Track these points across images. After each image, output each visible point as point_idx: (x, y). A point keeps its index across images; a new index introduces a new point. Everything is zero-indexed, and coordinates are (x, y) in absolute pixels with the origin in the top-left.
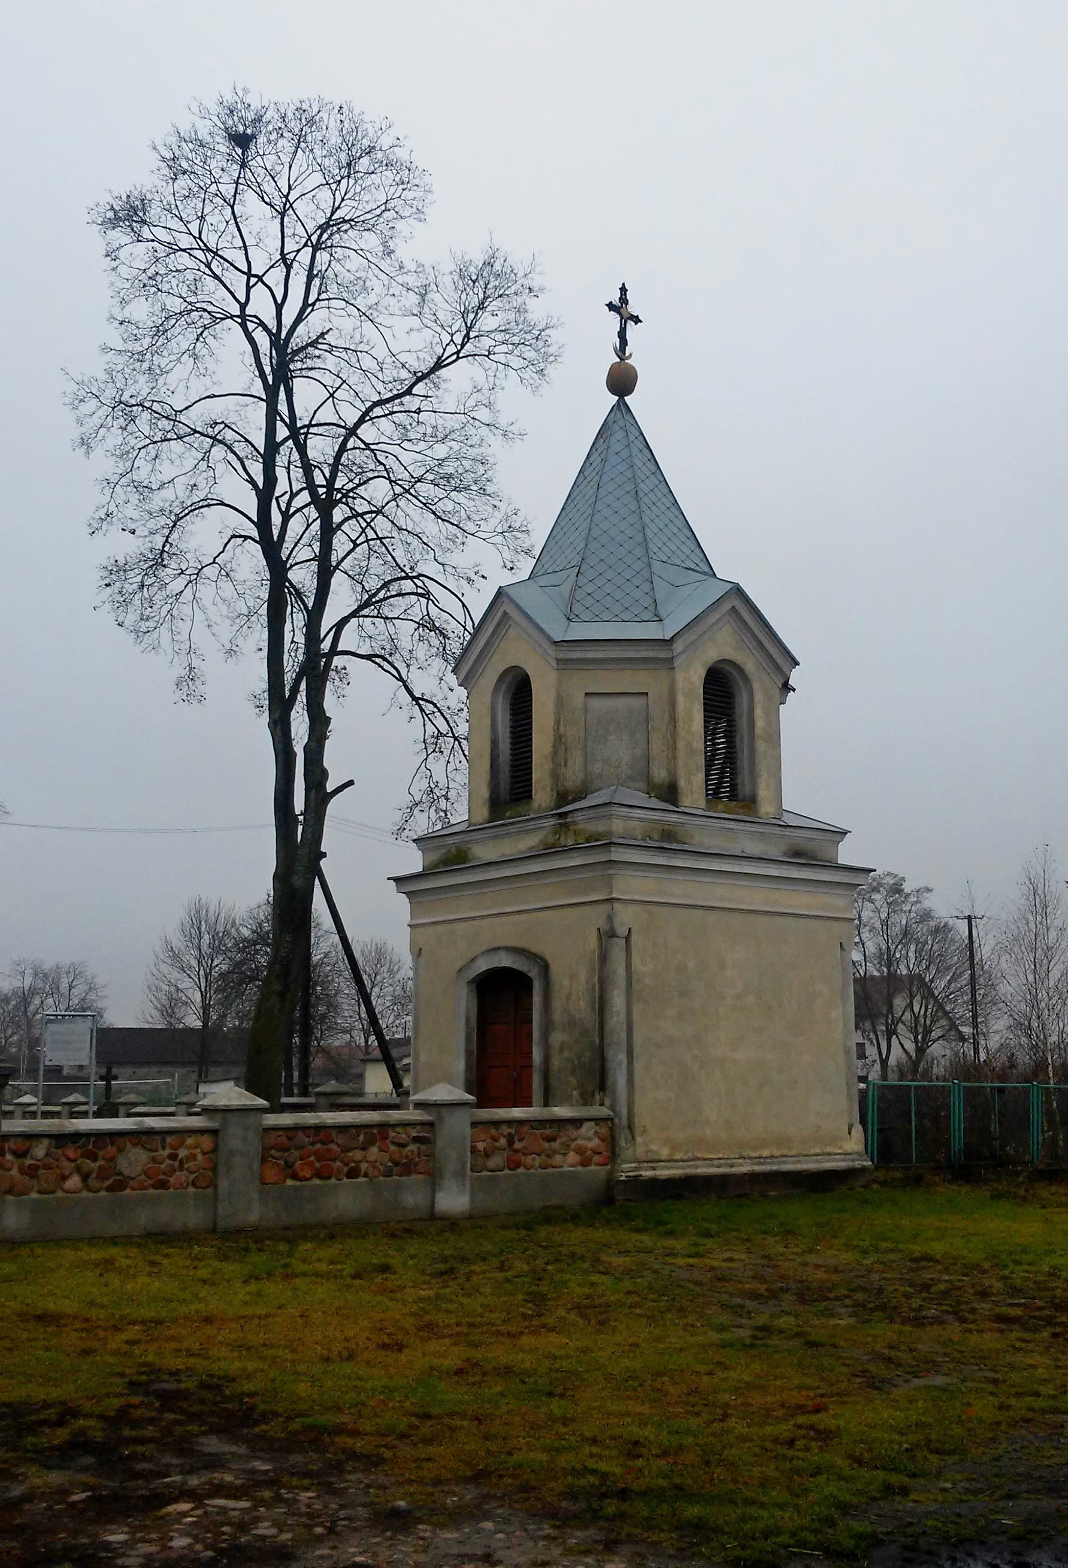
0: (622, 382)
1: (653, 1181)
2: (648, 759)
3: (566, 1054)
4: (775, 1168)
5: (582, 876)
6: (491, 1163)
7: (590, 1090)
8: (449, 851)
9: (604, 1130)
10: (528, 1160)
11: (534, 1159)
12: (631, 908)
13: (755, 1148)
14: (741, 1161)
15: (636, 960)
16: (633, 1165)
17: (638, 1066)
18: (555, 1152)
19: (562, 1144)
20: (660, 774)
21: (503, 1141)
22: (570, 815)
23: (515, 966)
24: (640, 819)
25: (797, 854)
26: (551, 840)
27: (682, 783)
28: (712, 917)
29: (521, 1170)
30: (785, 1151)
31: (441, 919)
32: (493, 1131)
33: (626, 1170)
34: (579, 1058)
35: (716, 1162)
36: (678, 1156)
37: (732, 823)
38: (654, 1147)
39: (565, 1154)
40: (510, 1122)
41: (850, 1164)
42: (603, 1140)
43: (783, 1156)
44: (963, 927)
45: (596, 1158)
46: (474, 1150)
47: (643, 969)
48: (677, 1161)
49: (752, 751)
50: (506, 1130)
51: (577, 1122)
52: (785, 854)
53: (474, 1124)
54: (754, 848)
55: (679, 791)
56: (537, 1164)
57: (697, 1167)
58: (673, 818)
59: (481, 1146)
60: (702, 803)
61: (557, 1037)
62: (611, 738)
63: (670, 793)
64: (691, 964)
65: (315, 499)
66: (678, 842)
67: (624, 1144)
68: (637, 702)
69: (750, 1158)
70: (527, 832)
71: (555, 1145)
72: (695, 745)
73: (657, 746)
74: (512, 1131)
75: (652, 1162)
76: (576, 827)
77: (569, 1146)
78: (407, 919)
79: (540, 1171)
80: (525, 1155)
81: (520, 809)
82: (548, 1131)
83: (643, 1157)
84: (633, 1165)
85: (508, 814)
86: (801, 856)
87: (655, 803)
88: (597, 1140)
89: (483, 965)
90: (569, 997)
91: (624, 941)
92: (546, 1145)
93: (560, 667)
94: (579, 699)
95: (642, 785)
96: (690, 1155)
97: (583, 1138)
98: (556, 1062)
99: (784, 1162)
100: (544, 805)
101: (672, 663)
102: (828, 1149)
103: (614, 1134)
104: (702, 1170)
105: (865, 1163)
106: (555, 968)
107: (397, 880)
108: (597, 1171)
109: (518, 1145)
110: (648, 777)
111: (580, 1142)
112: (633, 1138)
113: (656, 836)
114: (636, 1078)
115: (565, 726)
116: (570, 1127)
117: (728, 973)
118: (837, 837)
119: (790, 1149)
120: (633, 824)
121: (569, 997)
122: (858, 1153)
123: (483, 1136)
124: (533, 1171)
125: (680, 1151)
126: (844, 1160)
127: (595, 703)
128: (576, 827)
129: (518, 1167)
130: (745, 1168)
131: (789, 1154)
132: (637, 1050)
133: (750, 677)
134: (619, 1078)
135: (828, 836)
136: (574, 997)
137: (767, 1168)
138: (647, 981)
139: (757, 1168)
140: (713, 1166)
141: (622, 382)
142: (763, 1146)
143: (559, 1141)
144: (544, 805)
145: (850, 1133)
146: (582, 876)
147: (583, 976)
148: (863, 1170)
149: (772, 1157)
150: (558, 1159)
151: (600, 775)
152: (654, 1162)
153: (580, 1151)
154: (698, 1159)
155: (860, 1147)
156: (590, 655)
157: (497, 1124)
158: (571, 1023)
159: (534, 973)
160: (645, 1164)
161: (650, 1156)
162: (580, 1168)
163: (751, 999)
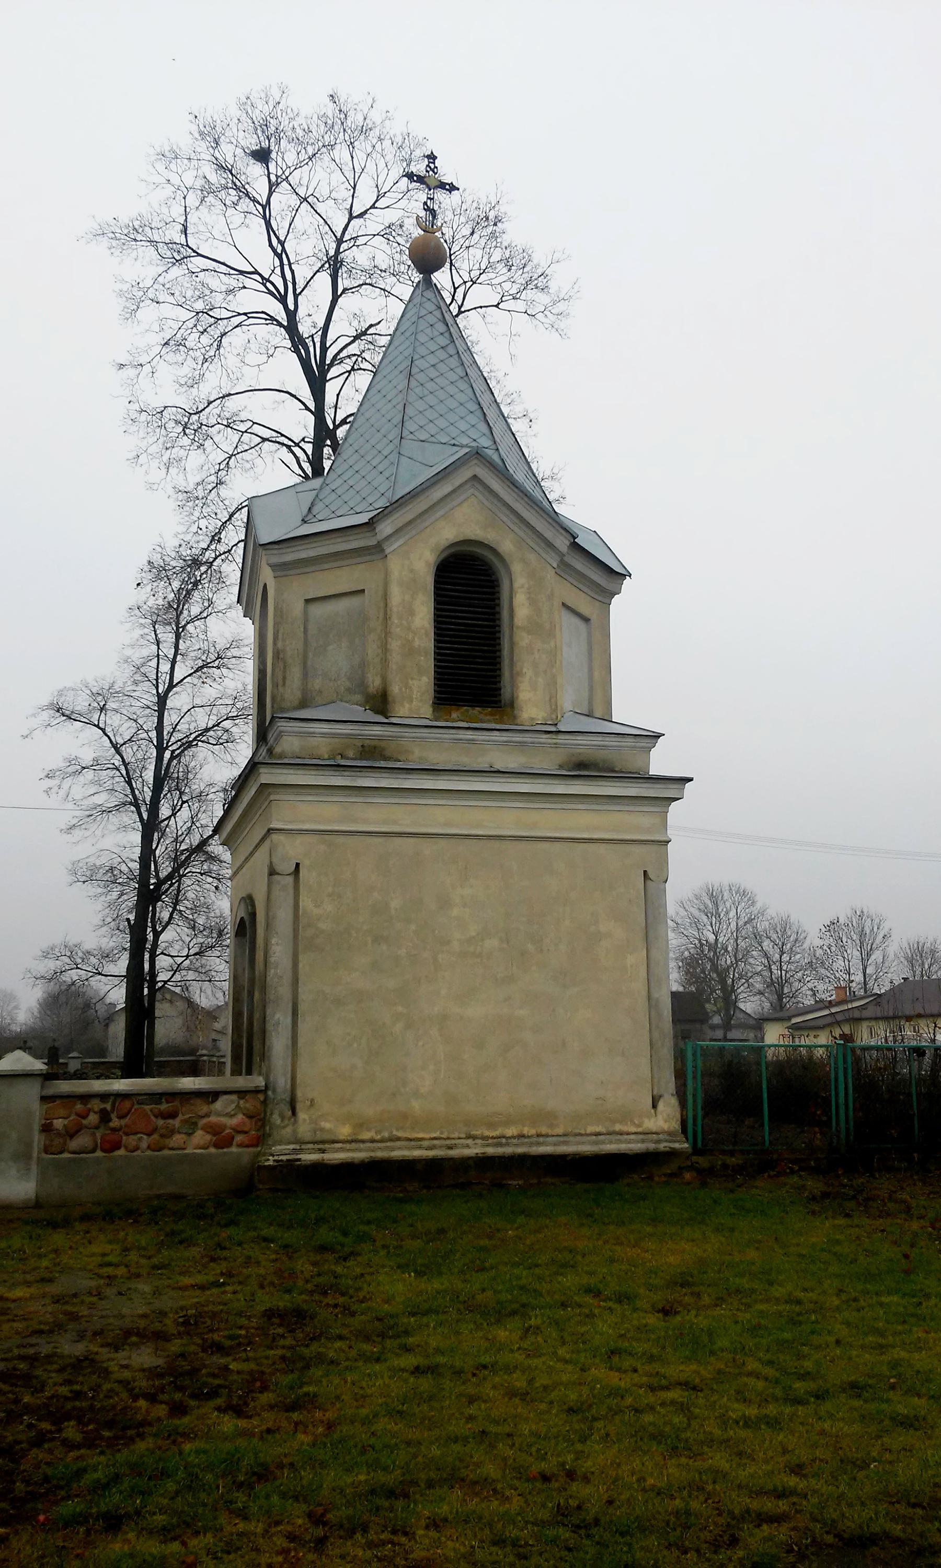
1: (317, 1167)
2: (363, 665)
4: (520, 1150)
6: (74, 1144)
9: (249, 1104)
10: (132, 1140)
11: (140, 1139)
12: (299, 839)
13: (491, 1125)
14: (469, 1141)
15: (306, 902)
16: (292, 1147)
17: (304, 1027)
18: (172, 1132)
19: (185, 1122)
20: (374, 683)
21: (93, 1118)
24: (324, 735)
25: (581, 765)
27: (395, 689)
28: (428, 848)
29: (122, 1152)
30: (544, 1130)
32: (79, 1107)
33: (279, 1152)
35: (426, 1143)
36: (366, 1135)
37: (470, 732)
38: (327, 1125)
39: (190, 1134)
40: (104, 1097)
41: (652, 1146)
42: (250, 1117)
43: (538, 1135)
45: (239, 1138)
46: (47, 1128)
47: (316, 911)
48: (363, 1141)
49: (512, 645)
50: (96, 1105)
51: (212, 1096)
52: (561, 767)
53: (44, 1099)
54: (512, 762)
55: (390, 699)
56: (144, 1145)
57: (393, 1149)
58: (377, 730)
59: (58, 1124)
60: (427, 710)
62: (331, 647)
63: (380, 703)
64: (395, 904)
65: (332, 434)
66: (386, 759)
67: (279, 1122)
68: (354, 601)
69: (484, 1138)
71: (176, 1123)
72: (417, 643)
73: (372, 650)
74: (108, 1106)
75: (323, 1142)
77: (195, 1124)
79: (149, 1153)
80: (127, 1134)
82: (164, 1106)
83: (308, 1136)
84: (292, 1147)
86: (583, 768)
87: (371, 716)
88: (240, 1116)
91: (290, 879)
92: (160, 1122)
93: (279, 573)
94: (299, 606)
95: (358, 697)
96: (386, 1135)
97: (219, 1114)
99: (539, 1144)
101: (383, 550)
102: (618, 1127)
103: (261, 1109)
104: (397, 1154)
105: (677, 1145)
108: (238, 1153)
109: (115, 1123)
110: (362, 685)
111: (213, 1119)
112: (294, 1113)
113: (351, 754)
114: (301, 1041)
115: (284, 640)
116: (199, 1101)
117: (455, 912)
118: (643, 743)
119: (551, 1126)
120: (314, 741)
122: (670, 1133)
123: (62, 1112)
124: (138, 1153)
125: (369, 1130)
126: (643, 1141)
127: (317, 611)
129: (119, 1148)
130: (474, 1150)
131: (550, 1132)
132: (302, 1008)
133: (507, 558)
134: (278, 1044)
135: (630, 742)
137: (508, 1150)
138: (322, 926)
139: (490, 1151)
140: (420, 1148)
142: (507, 1123)
143: (180, 1117)
145: (654, 1106)
148: (672, 1154)
149: (522, 1136)
150: (178, 1139)
151: (320, 692)
152: (322, 1143)
153: (215, 1130)
154: (399, 1139)
155: (675, 1125)
156: (303, 555)
157: (85, 1098)
160: (311, 1146)
161: (319, 1136)
162: (212, 1150)
163: (491, 943)
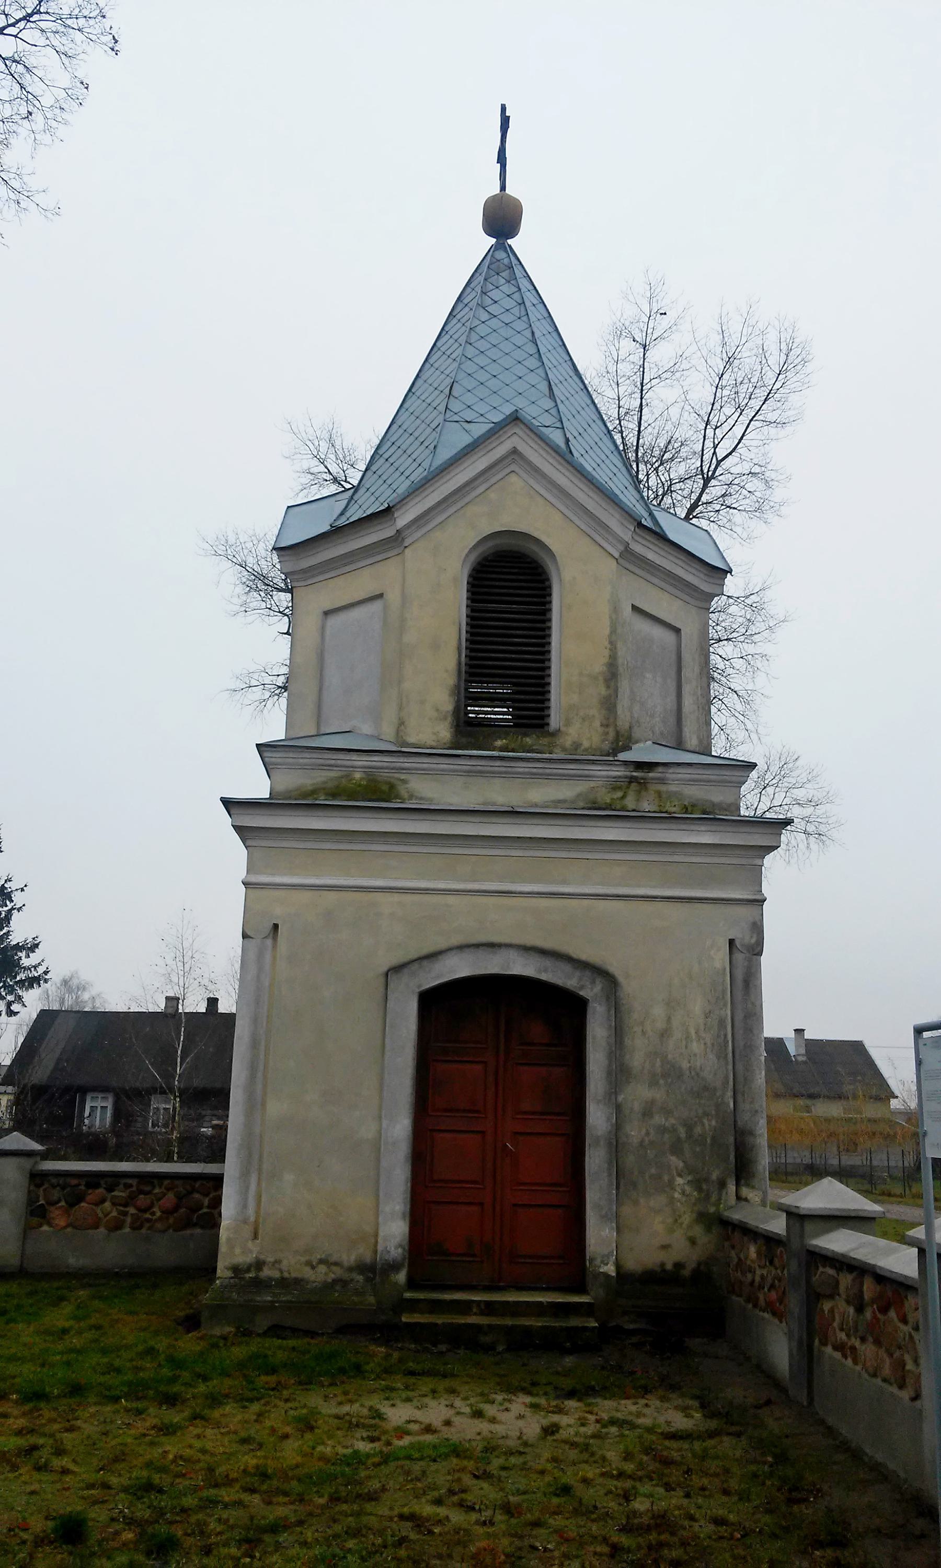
0: (502, 219)
3: (658, 1119)
5: (694, 859)
7: (714, 1176)
8: (348, 776)
22: (660, 769)
23: (544, 977)
26: (605, 797)
31: (441, 885)
34: (689, 1128)
44: (658, 1012)
61: (637, 1094)
70: (548, 777)
76: (663, 788)
78: (243, 874)
81: (528, 740)
85: (499, 743)
89: (460, 968)
90: (664, 1034)
98: (634, 1132)
100: (586, 744)
106: (629, 987)
107: (228, 804)
121: (664, 1034)
128: (663, 788)
136: (678, 1034)
141: (502, 219)
144: (586, 744)
146: (694, 859)
147: (697, 1006)
156: (650, 556)
158: (671, 1073)
159: (591, 991)
